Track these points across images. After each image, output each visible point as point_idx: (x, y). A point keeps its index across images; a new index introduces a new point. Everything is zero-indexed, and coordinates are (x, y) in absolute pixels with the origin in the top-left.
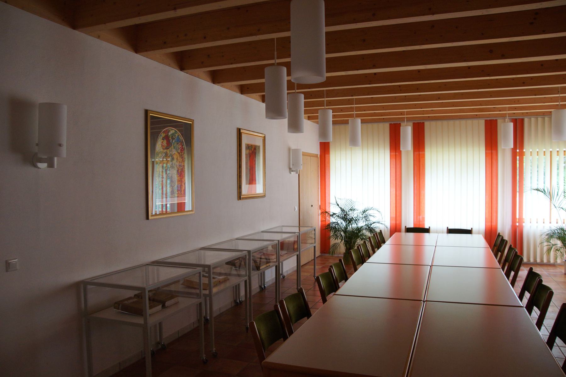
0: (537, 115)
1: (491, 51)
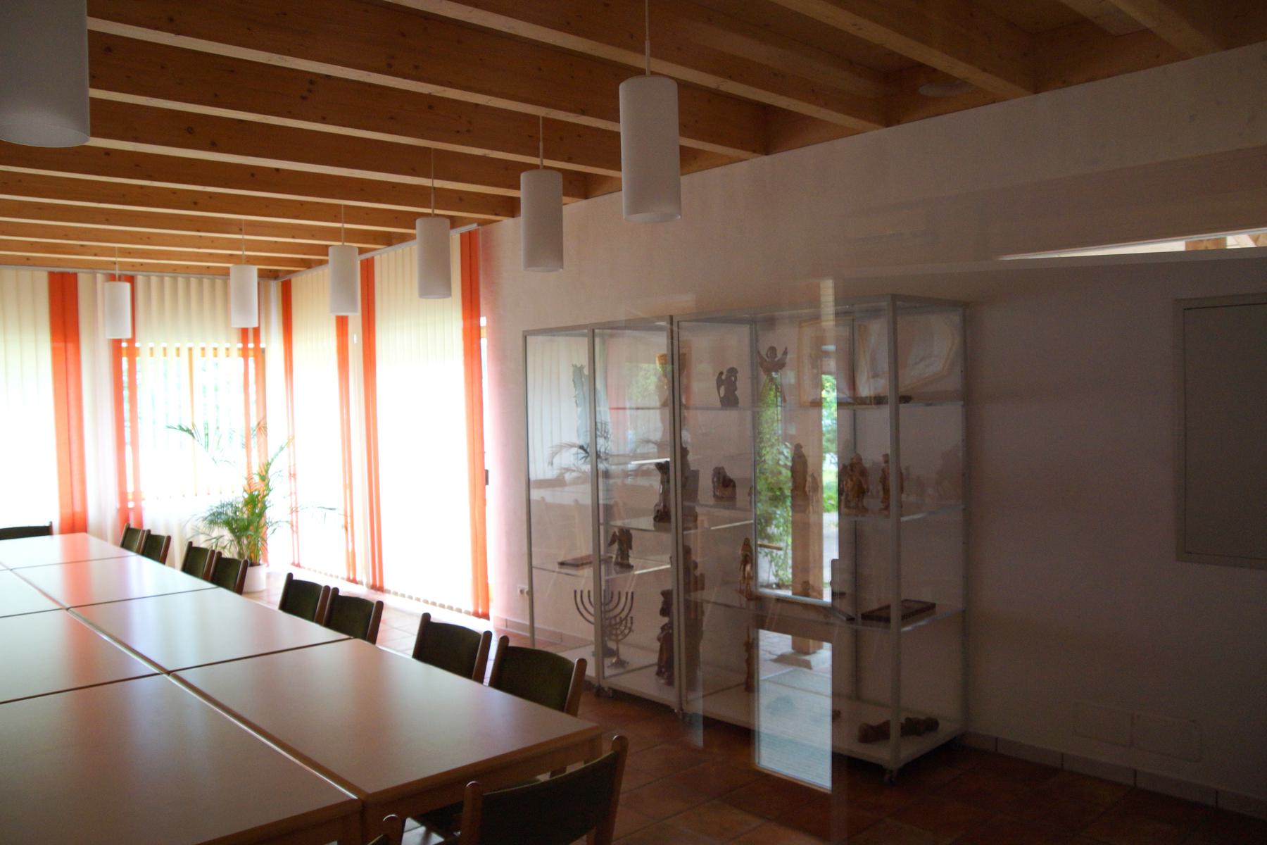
0: (162, 269)
1: (190, 131)
